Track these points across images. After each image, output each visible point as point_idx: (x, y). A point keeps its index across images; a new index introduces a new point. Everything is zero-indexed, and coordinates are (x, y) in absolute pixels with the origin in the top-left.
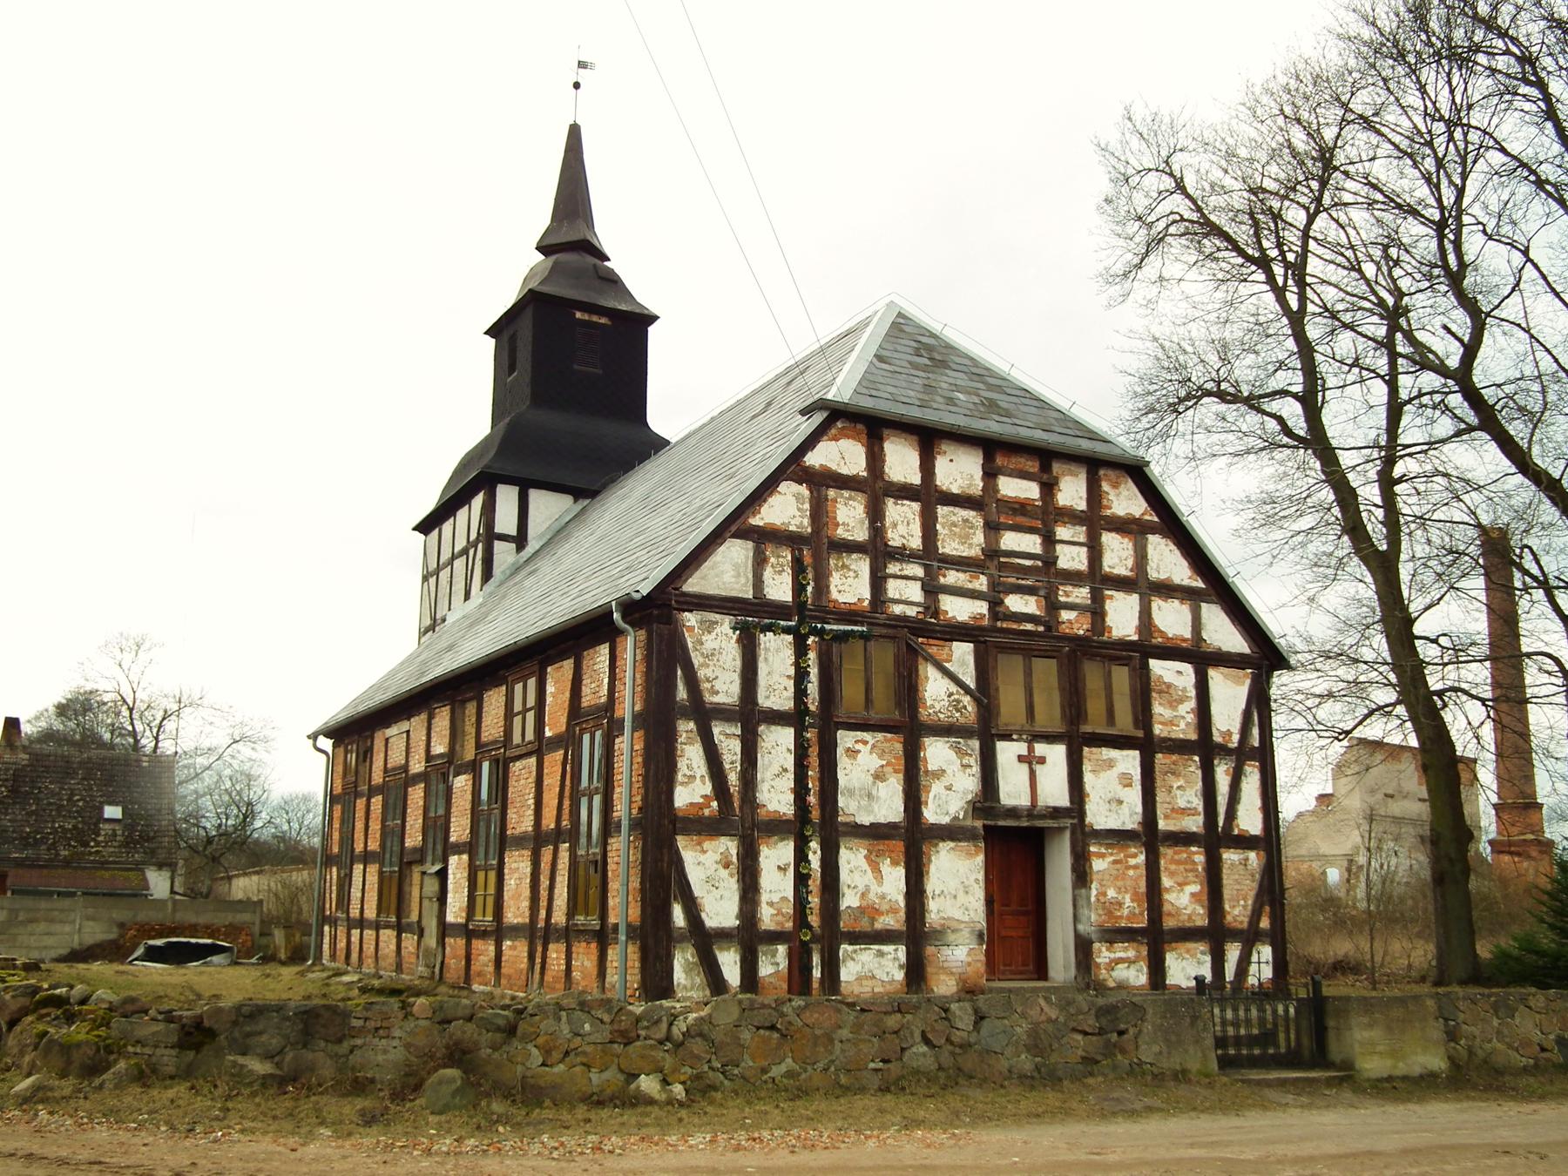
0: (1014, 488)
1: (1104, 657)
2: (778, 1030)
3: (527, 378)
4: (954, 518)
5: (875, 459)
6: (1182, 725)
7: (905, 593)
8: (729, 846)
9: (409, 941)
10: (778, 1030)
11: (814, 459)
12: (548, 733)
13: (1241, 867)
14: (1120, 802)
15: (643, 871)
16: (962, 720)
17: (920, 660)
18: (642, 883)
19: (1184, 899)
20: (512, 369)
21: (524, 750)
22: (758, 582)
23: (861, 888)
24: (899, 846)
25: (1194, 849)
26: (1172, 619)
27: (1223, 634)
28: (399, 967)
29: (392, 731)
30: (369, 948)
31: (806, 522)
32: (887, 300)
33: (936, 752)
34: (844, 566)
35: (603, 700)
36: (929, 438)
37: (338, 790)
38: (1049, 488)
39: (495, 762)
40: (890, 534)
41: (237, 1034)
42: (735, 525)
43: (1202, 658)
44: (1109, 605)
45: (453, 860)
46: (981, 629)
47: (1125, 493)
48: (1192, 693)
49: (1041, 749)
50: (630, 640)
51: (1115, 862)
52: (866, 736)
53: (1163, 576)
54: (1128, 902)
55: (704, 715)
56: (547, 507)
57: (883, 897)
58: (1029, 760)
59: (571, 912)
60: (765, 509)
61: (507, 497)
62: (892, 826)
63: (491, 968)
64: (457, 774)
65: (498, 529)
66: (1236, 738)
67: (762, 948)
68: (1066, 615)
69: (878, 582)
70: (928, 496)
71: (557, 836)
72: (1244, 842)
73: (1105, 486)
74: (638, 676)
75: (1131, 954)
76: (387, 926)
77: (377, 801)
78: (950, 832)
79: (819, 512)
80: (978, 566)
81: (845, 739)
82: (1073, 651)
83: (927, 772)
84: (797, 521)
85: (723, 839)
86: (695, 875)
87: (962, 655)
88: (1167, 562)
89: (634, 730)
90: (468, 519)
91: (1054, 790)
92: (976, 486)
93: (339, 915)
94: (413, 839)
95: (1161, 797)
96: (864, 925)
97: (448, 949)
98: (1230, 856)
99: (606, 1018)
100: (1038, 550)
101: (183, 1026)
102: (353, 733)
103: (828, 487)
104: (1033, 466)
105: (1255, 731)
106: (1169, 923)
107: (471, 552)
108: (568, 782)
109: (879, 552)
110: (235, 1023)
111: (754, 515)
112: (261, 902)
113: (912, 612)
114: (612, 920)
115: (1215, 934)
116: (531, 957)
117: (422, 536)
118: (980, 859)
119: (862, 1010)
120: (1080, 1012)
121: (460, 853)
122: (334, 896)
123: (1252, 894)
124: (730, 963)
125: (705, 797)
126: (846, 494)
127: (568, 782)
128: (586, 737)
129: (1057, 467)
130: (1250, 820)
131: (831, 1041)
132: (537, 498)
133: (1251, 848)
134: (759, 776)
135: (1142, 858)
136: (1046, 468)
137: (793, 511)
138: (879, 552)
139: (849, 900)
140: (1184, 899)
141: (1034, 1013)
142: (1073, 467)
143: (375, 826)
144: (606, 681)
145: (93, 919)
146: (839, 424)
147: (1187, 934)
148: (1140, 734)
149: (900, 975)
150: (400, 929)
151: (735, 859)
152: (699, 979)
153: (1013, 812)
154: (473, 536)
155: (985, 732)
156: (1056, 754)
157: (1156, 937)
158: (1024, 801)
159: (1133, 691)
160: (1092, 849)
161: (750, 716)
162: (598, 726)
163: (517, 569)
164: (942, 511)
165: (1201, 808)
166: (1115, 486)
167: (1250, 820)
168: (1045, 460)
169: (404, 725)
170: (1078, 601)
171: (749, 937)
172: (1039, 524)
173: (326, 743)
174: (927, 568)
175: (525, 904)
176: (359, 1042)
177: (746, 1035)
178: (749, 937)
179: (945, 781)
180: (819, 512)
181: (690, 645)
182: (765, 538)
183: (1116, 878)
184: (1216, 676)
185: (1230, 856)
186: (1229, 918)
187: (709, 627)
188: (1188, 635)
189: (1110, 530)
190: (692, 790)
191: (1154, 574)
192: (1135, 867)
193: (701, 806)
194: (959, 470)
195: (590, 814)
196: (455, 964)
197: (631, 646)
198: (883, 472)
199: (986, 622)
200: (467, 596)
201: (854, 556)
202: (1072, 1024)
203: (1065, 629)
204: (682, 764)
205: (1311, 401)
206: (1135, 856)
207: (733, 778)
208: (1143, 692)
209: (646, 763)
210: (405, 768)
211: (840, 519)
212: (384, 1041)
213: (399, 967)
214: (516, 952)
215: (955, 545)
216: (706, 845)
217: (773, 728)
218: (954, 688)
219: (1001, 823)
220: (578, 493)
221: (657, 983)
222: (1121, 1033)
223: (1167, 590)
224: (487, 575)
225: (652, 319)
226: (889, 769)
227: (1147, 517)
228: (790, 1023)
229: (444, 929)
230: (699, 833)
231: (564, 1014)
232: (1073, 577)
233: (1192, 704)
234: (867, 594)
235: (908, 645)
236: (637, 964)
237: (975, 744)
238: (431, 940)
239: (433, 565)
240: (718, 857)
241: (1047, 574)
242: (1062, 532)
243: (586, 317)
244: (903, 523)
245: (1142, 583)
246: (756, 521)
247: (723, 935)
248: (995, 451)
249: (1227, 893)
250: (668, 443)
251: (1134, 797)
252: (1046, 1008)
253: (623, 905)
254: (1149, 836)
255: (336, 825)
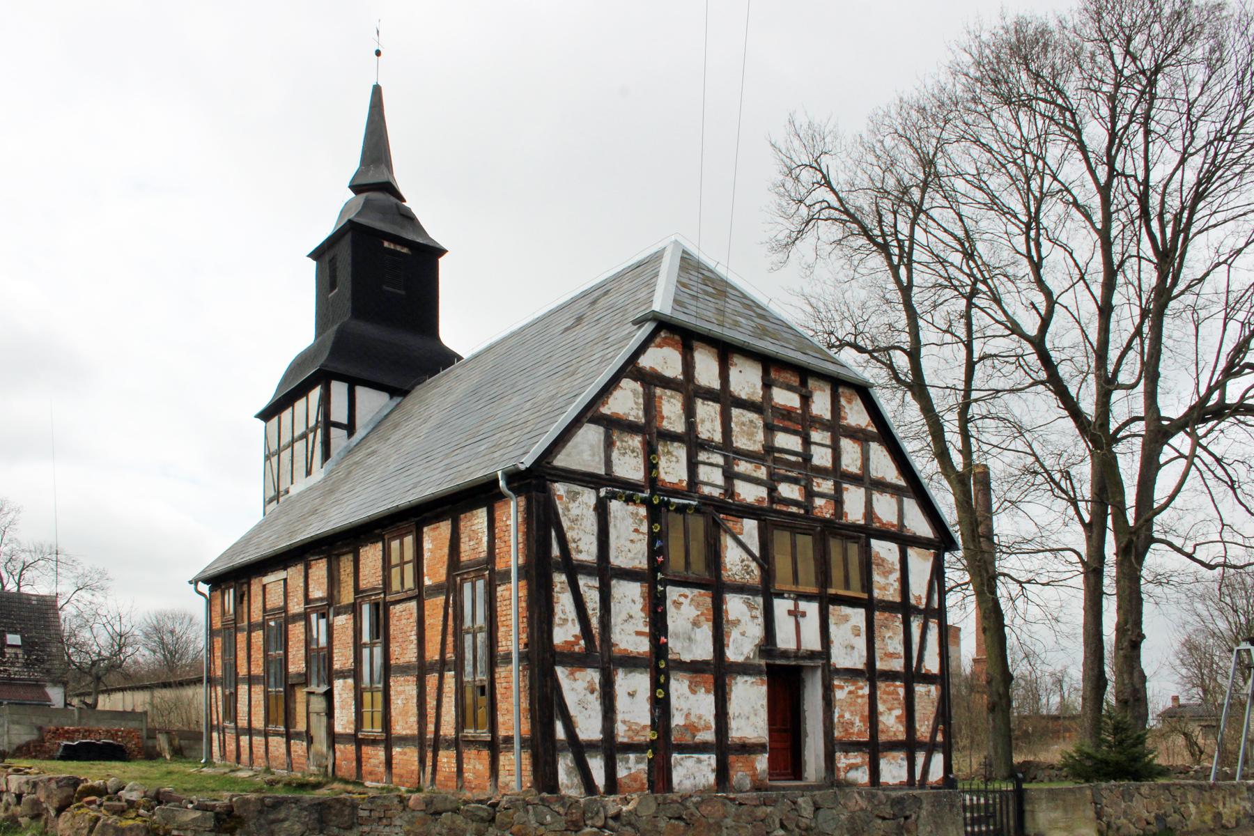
0: (785, 398)
1: (842, 535)
2: (682, 819)
3: (348, 294)
4: (743, 419)
5: (688, 366)
6: (892, 591)
7: (711, 476)
8: (593, 676)
9: (299, 747)
10: (682, 819)
11: (646, 361)
12: (427, 582)
13: (927, 695)
14: (853, 648)
15: (531, 694)
16: (751, 581)
17: (722, 532)
18: (531, 704)
19: (891, 722)
20: (333, 286)
21: (404, 596)
22: (608, 463)
23: (685, 712)
24: (709, 678)
25: (898, 683)
26: (885, 508)
27: (918, 524)
28: (290, 766)
29: (269, 579)
30: (259, 749)
31: (641, 414)
32: (673, 238)
33: (735, 605)
34: (669, 453)
35: (484, 555)
36: (726, 351)
37: (218, 624)
38: (806, 399)
39: (376, 607)
40: (700, 429)
41: (262, 821)
42: (590, 414)
43: (905, 540)
44: (846, 496)
45: (338, 684)
46: (762, 509)
47: (856, 408)
48: (898, 566)
49: (803, 605)
50: (512, 504)
51: (850, 692)
52: (686, 591)
53: (880, 476)
54: (857, 723)
55: (573, 570)
56: (371, 402)
57: (700, 718)
58: (796, 614)
59: (461, 724)
60: (611, 400)
61: (339, 390)
62: (705, 663)
63: (382, 769)
64: (337, 614)
65: (333, 418)
66: (924, 601)
67: (619, 756)
68: (819, 502)
69: (692, 466)
70: (725, 399)
71: (442, 666)
72: (928, 679)
73: (843, 402)
74: (520, 535)
75: (859, 760)
76: (277, 734)
77: (258, 636)
78: (744, 669)
79: (650, 406)
80: (760, 459)
81: (673, 593)
82: (822, 531)
83: (728, 621)
84: (633, 413)
85: (589, 671)
86: (570, 699)
87: (750, 528)
88: (883, 466)
89: (519, 579)
90: (307, 408)
91: (812, 641)
92: (757, 395)
93: (227, 724)
94: (297, 665)
95: (878, 644)
96: (688, 739)
97: (338, 754)
98: (920, 689)
99: (562, 811)
100: (799, 449)
101: (217, 814)
102: (231, 579)
103: (656, 386)
104: (795, 381)
105: (936, 597)
106: (882, 738)
107: (311, 436)
108: (451, 622)
109: (693, 443)
110: (261, 812)
111: (603, 405)
112: (145, 713)
113: (716, 493)
114: (502, 733)
115: (909, 745)
116: (422, 761)
117: (262, 423)
118: (764, 688)
119: (740, 804)
120: (880, 803)
121: (345, 677)
122: (220, 709)
123: (933, 716)
124: (597, 766)
125: (575, 636)
126: (668, 392)
127: (451, 622)
128: (467, 587)
129: (812, 383)
130: (932, 664)
131: (720, 827)
132: (362, 393)
133: (932, 683)
134: (613, 621)
135: (866, 691)
136: (804, 383)
137: (631, 404)
138: (693, 443)
139: (677, 720)
140: (891, 722)
141: (851, 804)
142: (822, 384)
143: (258, 656)
144: (485, 539)
145: (18, 723)
146: (663, 334)
147: (893, 746)
148: (865, 596)
149: (712, 778)
150: (289, 736)
151: (597, 687)
152: (577, 780)
153: (785, 654)
154: (312, 423)
155: (767, 591)
156: (812, 609)
157: (874, 748)
158: (792, 646)
159: (861, 563)
160: (836, 682)
161: (605, 572)
162: (478, 577)
163: (350, 452)
164: (735, 412)
165: (902, 654)
166: (849, 402)
167: (932, 664)
168: (803, 375)
169: (282, 575)
170: (826, 491)
171: (611, 748)
172: (799, 428)
173: (205, 588)
174: (725, 457)
175: (413, 719)
176: (366, 829)
177: (662, 824)
178: (611, 748)
179: (741, 628)
180: (650, 406)
181: (560, 511)
182: (614, 425)
183: (850, 705)
184: (912, 553)
185: (920, 689)
186: (918, 734)
187: (574, 496)
188: (895, 522)
189: (846, 437)
190: (565, 632)
191: (874, 474)
192: (862, 697)
193: (572, 644)
194: (746, 380)
195: (475, 645)
196: (346, 765)
197: (512, 513)
198: (693, 377)
199: (766, 504)
200: (308, 473)
201: (676, 444)
202: (876, 812)
203: (817, 512)
204: (558, 609)
205: (914, 355)
206: (862, 688)
207: (595, 622)
208: (867, 563)
209: (530, 607)
210: (285, 609)
211: (665, 413)
212: (387, 829)
213: (290, 766)
214: (406, 757)
215: (744, 440)
216: (578, 674)
217: (622, 582)
218: (745, 556)
219: (778, 662)
220: (398, 391)
221: (545, 779)
222: (906, 818)
223: (881, 486)
224: (326, 455)
225: (441, 252)
226: (702, 618)
227: (870, 428)
228: (692, 814)
229: (333, 738)
230: (572, 666)
231: (530, 807)
232: (822, 472)
233: (897, 575)
234: (685, 477)
235: (714, 520)
236: (529, 768)
237: (760, 600)
238: (321, 745)
239: (274, 447)
240: (586, 685)
241: (805, 468)
242: (816, 436)
243: (392, 247)
244: (708, 418)
245: (866, 479)
246: (605, 410)
247: (592, 746)
248: (769, 364)
249: (917, 715)
250: (460, 358)
251: (861, 643)
252: (860, 801)
253: (513, 717)
254: (871, 674)
255: (218, 653)
